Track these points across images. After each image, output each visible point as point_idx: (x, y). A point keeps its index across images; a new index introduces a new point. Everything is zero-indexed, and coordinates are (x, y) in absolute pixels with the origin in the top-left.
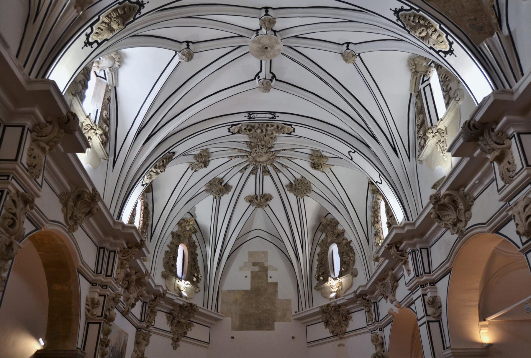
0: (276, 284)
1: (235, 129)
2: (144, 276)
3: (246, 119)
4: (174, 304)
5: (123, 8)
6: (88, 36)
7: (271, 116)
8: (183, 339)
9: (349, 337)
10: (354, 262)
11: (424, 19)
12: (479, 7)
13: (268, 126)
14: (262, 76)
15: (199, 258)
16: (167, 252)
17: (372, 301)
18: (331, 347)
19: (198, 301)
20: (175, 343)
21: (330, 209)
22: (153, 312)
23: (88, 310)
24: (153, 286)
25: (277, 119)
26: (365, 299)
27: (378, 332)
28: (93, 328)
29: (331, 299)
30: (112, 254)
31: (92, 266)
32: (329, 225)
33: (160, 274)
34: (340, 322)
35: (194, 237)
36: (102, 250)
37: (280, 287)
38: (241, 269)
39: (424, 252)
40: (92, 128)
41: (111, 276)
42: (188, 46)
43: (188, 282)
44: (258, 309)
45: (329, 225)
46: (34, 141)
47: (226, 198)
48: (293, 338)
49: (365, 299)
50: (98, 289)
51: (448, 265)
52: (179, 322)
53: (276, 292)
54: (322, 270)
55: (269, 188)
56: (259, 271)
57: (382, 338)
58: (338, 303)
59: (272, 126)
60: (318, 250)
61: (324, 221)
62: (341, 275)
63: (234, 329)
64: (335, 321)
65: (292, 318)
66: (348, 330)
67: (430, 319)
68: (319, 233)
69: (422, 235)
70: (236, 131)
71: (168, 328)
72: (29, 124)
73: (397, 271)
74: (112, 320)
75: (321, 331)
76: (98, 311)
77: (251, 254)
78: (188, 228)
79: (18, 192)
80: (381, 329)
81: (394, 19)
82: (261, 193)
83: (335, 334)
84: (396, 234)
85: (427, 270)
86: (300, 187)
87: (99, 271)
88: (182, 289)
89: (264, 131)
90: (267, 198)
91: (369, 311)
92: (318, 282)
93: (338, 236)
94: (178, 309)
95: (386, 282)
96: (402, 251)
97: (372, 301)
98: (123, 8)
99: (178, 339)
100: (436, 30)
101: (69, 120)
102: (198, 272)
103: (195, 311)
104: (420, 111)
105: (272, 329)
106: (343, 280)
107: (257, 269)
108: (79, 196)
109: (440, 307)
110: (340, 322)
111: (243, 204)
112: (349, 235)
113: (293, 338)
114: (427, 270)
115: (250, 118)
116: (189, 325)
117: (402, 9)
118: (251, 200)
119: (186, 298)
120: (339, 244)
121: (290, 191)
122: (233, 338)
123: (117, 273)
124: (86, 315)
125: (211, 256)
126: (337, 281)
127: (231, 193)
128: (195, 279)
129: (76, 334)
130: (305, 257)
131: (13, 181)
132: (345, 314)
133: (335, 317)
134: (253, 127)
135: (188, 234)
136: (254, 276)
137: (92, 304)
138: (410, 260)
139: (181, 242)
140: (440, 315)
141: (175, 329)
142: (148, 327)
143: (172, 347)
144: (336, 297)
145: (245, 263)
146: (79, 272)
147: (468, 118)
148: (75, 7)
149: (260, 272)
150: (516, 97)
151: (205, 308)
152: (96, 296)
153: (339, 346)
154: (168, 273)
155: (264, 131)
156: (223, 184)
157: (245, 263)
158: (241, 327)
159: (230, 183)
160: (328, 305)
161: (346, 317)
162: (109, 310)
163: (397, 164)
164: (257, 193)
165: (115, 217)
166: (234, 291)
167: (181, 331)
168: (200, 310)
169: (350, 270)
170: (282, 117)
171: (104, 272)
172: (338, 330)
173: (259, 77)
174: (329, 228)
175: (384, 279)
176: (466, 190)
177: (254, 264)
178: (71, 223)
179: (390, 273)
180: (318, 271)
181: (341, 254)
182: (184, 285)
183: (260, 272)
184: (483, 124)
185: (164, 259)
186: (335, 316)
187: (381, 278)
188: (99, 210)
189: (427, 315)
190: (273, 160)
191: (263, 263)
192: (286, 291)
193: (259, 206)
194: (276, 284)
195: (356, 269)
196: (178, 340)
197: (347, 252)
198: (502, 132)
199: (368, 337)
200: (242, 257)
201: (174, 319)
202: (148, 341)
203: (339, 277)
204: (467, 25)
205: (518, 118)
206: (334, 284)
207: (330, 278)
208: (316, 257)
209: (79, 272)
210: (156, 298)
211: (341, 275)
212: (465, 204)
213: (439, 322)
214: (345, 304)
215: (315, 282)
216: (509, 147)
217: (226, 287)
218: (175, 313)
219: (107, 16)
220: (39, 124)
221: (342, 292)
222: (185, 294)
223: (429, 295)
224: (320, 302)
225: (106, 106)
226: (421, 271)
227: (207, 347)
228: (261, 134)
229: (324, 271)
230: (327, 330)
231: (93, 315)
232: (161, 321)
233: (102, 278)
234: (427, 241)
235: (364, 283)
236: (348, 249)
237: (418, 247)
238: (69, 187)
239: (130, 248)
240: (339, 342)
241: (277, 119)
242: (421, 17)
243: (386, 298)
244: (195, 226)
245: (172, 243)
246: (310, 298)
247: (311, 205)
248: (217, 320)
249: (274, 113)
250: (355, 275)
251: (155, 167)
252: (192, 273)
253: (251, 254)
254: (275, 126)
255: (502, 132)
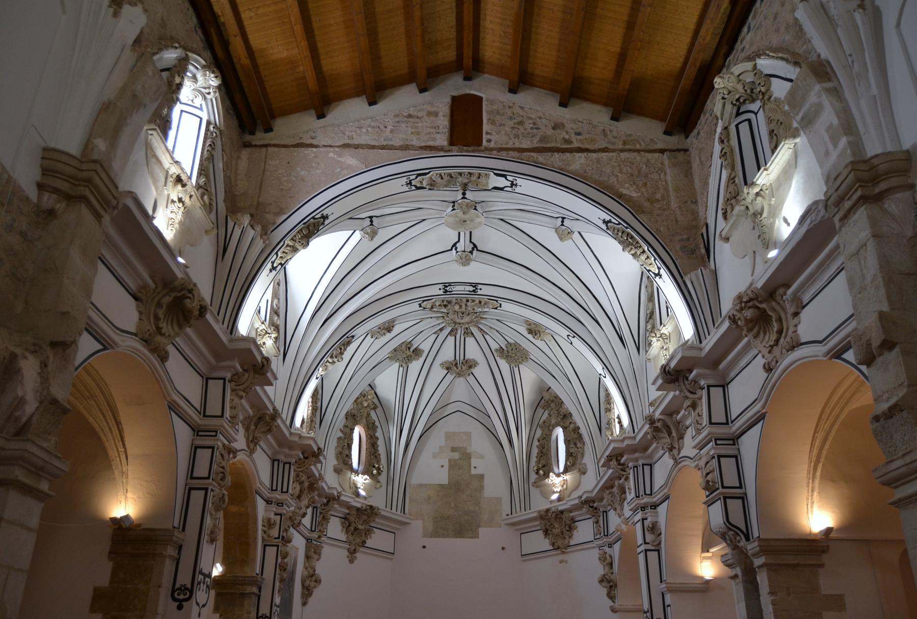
0: (481, 477)
1: (428, 304)
2: (317, 480)
3: (441, 292)
4: (349, 507)
5: (308, 227)
6: (273, 263)
7: (472, 289)
8: (361, 549)
9: (572, 552)
10: (583, 455)
11: (632, 237)
12: (694, 223)
13: (467, 301)
14: (460, 247)
15: (381, 443)
16: (339, 439)
17: (601, 510)
18: (550, 563)
19: (379, 502)
20: (352, 553)
21: (550, 382)
22: (325, 519)
23: (265, 532)
24: (326, 488)
25: (479, 292)
26: (592, 507)
27: (606, 549)
28: (271, 552)
29: (552, 502)
30: (287, 466)
31: (267, 482)
32: (552, 401)
33: (332, 469)
34: (562, 533)
35: (373, 413)
36: (276, 463)
37: (487, 482)
38: (435, 456)
39: (647, 468)
40: (267, 333)
41: (287, 492)
42: (371, 221)
43: (366, 476)
44: (457, 510)
45: (552, 401)
46: (233, 390)
47: (415, 366)
48: (503, 548)
49: (592, 507)
50: (274, 508)
51: (665, 491)
52: (356, 529)
53: (481, 488)
54: (543, 462)
55: (472, 351)
56: (460, 459)
57: (611, 556)
58: (560, 508)
59: (473, 301)
60: (539, 433)
61: (547, 396)
62: (566, 471)
63: (426, 535)
64: (556, 531)
65: (502, 523)
66: (572, 543)
67: (649, 547)
68: (540, 411)
69: (646, 449)
70: (429, 306)
71: (343, 537)
72: (228, 376)
73: (653, 451)
74: (289, 541)
75: (538, 541)
76: (275, 532)
77: (448, 435)
78: (365, 404)
79: (224, 445)
80: (610, 545)
81: (604, 227)
82: (462, 358)
83: (556, 547)
84: (614, 448)
85: (648, 492)
86: (514, 354)
87: (274, 488)
88: (359, 485)
89: (464, 306)
90: (470, 365)
91: (597, 522)
92: (537, 476)
93: (565, 419)
94: (354, 512)
95: (612, 490)
96: (623, 465)
97: (601, 510)
98: (308, 227)
99: (355, 550)
100: (644, 252)
101: (263, 366)
102: (379, 461)
103: (376, 514)
104: (651, 299)
105: (476, 536)
106: (568, 477)
107: (456, 455)
108: (260, 418)
109: (660, 534)
110: (562, 533)
111: (438, 373)
112: (577, 418)
113: (503, 548)
114: (648, 492)
115: (446, 291)
116: (368, 532)
117: (610, 221)
118: (449, 367)
119: (365, 498)
120: (565, 429)
121: (501, 357)
122: (424, 547)
123: (294, 488)
124: (263, 538)
125: (395, 440)
126: (561, 479)
127: (422, 359)
128: (375, 472)
129: (254, 559)
130: (521, 441)
131: (221, 437)
132: (568, 522)
133: (556, 526)
134: (449, 302)
135: (365, 412)
136: (453, 465)
137: (269, 524)
138: (631, 476)
139: (356, 423)
140: (660, 544)
141: (351, 538)
142: (319, 537)
143: (347, 560)
144: (559, 499)
145: (441, 447)
146: (257, 493)
147: (664, 362)
148: (261, 237)
149: (461, 460)
150: (703, 354)
151: (388, 509)
152: (272, 516)
153: (561, 562)
154: (342, 466)
155: (464, 306)
156: (412, 350)
157: (441, 447)
158: (435, 534)
159: (421, 347)
160: (548, 510)
161: (570, 527)
162: (286, 531)
163: (623, 356)
164: (457, 358)
165: (288, 423)
166: (426, 486)
167: (358, 540)
168: (383, 513)
169: (578, 466)
170: (485, 290)
171: (279, 488)
172: (560, 542)
173: (456, 249)
174: (553, 405)
175: (612, 487)
176: (679, 417)
177: (454, 450)
178: (252, 446)
179: (616, 483)
180: (538, 462)
181: (567, 442)
182: (361, 481)
183: (461, 460)
184: (677, 371)
185: (336, 447)
186: (557, 525)
187: (608, 486)
188: (278, 427)
189: (645, 543)
190: (477, 322)
191: (465, 449)
192: (495, 487)
193: (459, 375)
194: (481, 477)
195: (585, 464)
196: (355, 551)
197: (574, 439)
198: (695, 381)
199: (595, 554)
200: (437, 439)
201: (350, 525)
202: (320, 555)
203: (563, 473)
204: (678, 248)
205: (707, 371)
206: (556, 482)
207: (551, 474)
208: (536, 443)
209: (257, 493)
210: (328, 502)
211: (566, 471)
212: (678, 430)
213: (658, 551)
214: (570, 511)
215: (533, 477)
216: (700, 399)
217: (415, 480)
218: (352, 519)
219: (292, 239)
220: (236, 374)
221: (567, 493)
222: (362, 493)
223: (649, 519)
224: (539, 505)
225: (275, 295)
226: (642, 493)
227: (392, 559)
228: (460, 308)
229: (545, 466)
230: (547, 541)
231: (269, 536)
232: (335, 528)
233: (277, 496)
234: (650, 457)
235: (590, 488)
236: (575, 436)
237: (640, 462)
238: (251, 412)
239: (306, 458)
240: (561, 557)
241: (479, 292)
242: (628, 234)
243: (615, 509)
244: (376, 400)
245: (345, 426)
246: (527, 497)
247: (528, 376)
248: (404, 524)
249: (475, 285)
250: (583, 472)
251: (332, 357)
252: (371, 465)
253: (448, 435)
254: (477, 301)
255: (695, 381)
